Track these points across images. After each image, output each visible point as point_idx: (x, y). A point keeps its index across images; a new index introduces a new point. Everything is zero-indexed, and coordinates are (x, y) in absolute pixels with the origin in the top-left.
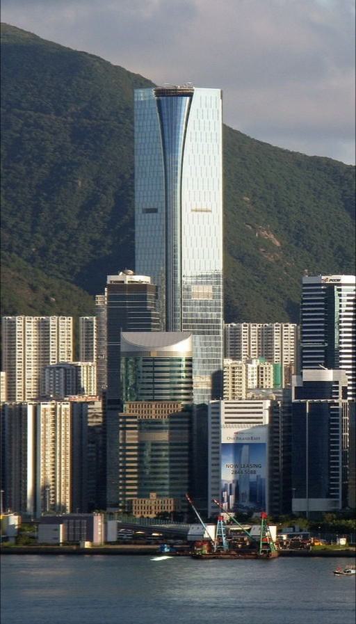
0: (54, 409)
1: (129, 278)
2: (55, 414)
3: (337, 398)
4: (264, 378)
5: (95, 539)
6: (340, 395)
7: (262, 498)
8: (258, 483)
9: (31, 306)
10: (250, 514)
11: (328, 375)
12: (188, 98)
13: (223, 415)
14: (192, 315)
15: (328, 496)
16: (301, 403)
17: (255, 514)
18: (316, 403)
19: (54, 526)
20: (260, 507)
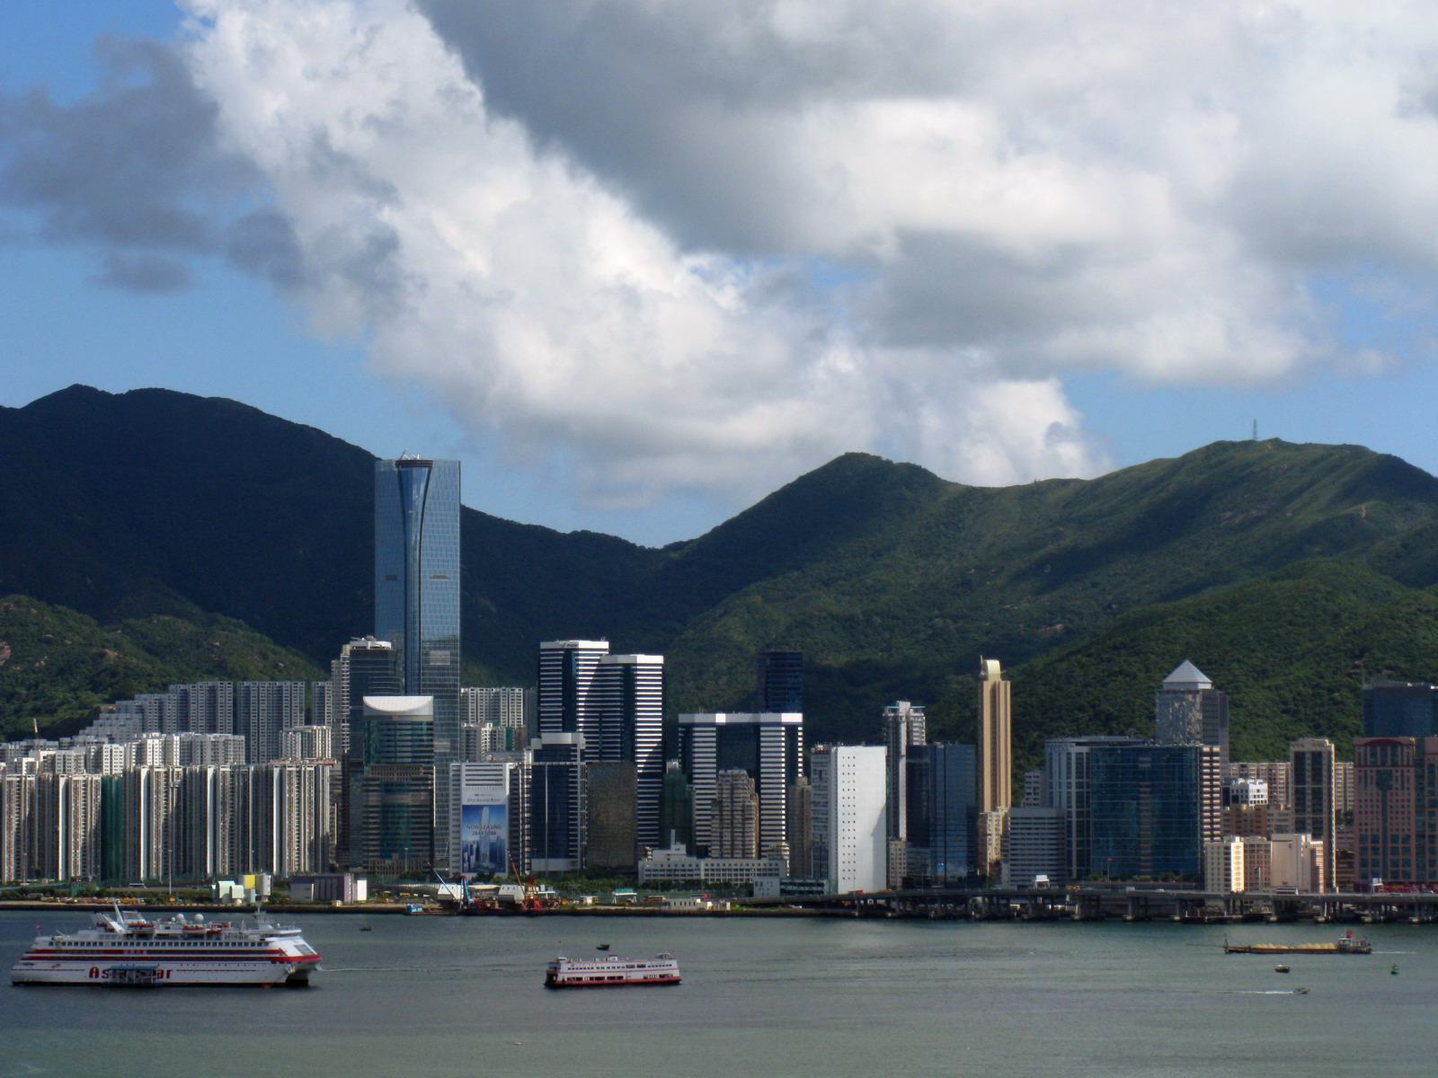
0: (299, 772)
1: (370, 643)
2: (299, 776)
3: (575, 761)
4: (497, 741)
5: (345, 897)
6: (579, 759)
7: (502, 858)
8: (498, 845)
9: (261, 672)
10: (492, 872)
11: (568, 738)
12: (427, 469)
13: (464, 778)
14: (430, 680)
15: (567, 856)
16: (540, 766)
17: (497, 875)
18: (555, 761)
19: (306, 886)
20: (501, 867)
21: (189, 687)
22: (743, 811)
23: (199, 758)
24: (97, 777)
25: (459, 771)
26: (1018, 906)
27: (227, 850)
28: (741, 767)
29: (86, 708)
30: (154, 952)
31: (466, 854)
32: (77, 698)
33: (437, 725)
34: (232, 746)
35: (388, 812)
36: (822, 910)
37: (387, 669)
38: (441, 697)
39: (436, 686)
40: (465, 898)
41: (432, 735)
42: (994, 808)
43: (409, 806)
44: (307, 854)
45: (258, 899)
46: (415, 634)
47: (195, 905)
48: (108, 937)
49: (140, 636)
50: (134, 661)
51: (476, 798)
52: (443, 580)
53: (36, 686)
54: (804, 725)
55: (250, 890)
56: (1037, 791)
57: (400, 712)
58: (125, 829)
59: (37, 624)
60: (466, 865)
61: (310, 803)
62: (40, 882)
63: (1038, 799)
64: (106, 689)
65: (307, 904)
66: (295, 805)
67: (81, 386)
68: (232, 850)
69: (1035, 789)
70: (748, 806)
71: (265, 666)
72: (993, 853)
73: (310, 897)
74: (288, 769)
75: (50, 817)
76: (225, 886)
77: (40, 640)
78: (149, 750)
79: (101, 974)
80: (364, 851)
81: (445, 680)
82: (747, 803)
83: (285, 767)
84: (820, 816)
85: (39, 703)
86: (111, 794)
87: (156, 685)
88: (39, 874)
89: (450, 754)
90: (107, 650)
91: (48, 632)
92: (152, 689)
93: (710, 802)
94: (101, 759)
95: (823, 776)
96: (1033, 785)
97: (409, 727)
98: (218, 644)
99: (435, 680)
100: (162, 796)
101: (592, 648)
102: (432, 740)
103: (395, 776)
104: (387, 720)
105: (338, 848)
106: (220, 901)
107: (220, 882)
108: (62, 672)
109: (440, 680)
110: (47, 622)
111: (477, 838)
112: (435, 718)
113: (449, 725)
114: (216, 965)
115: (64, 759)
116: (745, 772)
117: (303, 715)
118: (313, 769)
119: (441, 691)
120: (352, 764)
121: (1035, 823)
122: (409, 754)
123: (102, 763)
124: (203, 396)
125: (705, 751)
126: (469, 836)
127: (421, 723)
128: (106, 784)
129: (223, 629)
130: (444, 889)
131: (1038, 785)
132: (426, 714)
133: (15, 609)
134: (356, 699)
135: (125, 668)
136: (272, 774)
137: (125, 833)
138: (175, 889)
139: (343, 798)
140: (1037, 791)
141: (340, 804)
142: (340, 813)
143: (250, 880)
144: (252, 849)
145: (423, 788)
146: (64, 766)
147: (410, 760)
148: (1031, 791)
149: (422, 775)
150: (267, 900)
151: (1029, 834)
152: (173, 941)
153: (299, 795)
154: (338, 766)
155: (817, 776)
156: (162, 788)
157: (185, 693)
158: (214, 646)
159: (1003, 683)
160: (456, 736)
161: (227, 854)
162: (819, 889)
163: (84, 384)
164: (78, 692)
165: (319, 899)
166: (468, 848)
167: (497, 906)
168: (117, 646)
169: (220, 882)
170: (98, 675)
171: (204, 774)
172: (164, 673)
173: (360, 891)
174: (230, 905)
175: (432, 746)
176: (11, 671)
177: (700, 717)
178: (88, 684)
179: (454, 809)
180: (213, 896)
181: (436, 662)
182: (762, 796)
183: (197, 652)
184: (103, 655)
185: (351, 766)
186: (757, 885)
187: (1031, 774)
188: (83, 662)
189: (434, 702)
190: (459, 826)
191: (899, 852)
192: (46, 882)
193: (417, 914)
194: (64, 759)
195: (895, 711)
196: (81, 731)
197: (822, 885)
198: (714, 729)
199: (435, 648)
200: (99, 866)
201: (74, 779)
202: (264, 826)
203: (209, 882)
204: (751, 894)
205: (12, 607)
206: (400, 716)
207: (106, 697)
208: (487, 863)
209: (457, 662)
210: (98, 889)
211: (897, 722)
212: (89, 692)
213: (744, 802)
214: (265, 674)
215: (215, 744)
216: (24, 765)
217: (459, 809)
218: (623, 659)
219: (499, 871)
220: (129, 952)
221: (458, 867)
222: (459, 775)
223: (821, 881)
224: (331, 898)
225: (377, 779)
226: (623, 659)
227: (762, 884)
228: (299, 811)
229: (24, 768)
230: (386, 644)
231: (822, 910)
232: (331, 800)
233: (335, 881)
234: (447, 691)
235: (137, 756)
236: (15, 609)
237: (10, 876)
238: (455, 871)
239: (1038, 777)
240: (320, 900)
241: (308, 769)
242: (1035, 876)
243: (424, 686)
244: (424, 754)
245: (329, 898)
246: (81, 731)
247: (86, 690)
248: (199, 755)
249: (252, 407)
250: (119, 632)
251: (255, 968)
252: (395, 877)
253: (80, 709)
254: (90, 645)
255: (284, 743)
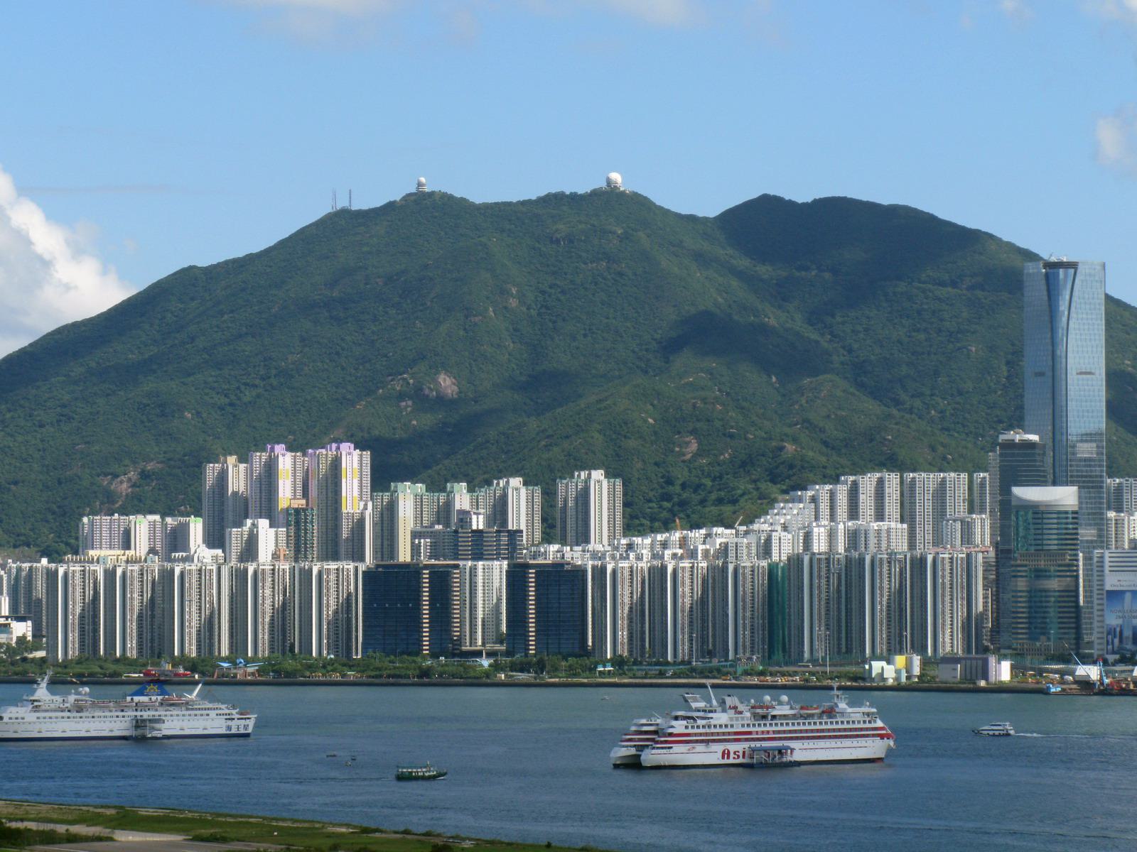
1: (1018, 436)
2: (952, 562)
14: (1077, 471)
19: (953, 666)
21: (860, 478)
23: (863, 546)
24: (764, 563)
25: (1102, 557)
27: (884, 632)
29: (765, 498)
30: (779, 732)
31: (1110, 637)
32: (758, 489)
33: (1084, 514)
35: (1036, 598)
37: (1035, 461)
38: (1084, 487)
39: (1082, 476)
40: (1101, 681)
41: (1077, 523)
43: (1055, 591)
44: (960, 636)
45: (908, 678)
46: (1062, 427)
47: (849, 684)
48: (737, 719)
49: (818, 430)
50: (811, 454)
51: (1118, 583)
52: (1088, 376)
53: (721, 477)
55: (900, 670)
57: (1046, 501)
58: (789, 612)
59: (722, 420)
60: (1110, 647)
61: (962, 588)
62: (710, 662)
64: (783, 480)
65: (954, 683)
66: (948, 590)
67: (769, 195)
68: (889, 632)
71: (934, 458)
73: (956, 677)
74: (941, 556)
75: (721, 599)
76: (877, 666)
77: (724, 435)
78: (815, 538)
79: (732, 755)
80: (1013, 633)
81: (1091, 471)
83: (938, 553)
85: (723, 493)
86: (777, 579)
87: (831, 477)
88: (711, 654)
89: (1096, 541)
90: (786, 444)
91: (732, 428)
92: (826, 480)
94: (771, 546)
97: (1055, 516)
98: (890, 437)
99: (1082, 471)
100: (824, 581)
102: (1076, 529)
103: (1043, 562)
104: (1038, 512)
105: (992, 631)
106: (873, 680)
107: (872, 662)
108: (743, 464)
109: (1087, 471)
110: (731, 417)
111: (1120, 622)
112: (1080, 508)
113: (1094, 514)
114: (832, 743)
115: (737, 546)
117: (966, 504)
118: (964, 556)
119: (1084, 482)
122: (1056, 542)
123: (771, 550)
124: (884, 203)
126: (1113, 620)
127: (1066, 512)
128: (772, 569)
129: (896, 424)
130: (1082, 670)
132: (1071, 503)
133: (702, 406)
134: (1005, 489)
135: (802, 460)
136: (802, 561)
137: (790, 616)
138: (834, 669)
139: (997, 584)
141: (994, 589)
142: (994, 598)
143: (900, 660)
144: (906, 629)
145: (1068, 574)
146: (736, 553)
147: (1056, 547)
149: (1067, 561)
150: (916, 680)
152: (785, 722)
153: (952, 581)
154: (992, 554)
156: (823, 573)
157: (855, 484)
158: (885, 439)
160: (1103, 525)
161: (884, 636)
163: (772, 194)
164: (758, 483)
165: (965, 679)
166: (1111, 631)
167: (1132, 687)
168: (795, 440)
169: (872, 662)
170: (777, 467)
171: (310, 570)
172: (838, 466)
173: (1003, 671)
174: (881, 684)
175: (1077, 534)
176: (697, 464)
178: (768, 475)
179: (1098, 594)
180: (867, 676)
181: (1083, 453)
183: (870, 445)
184: (782, 449)
185: (1003, 553)
188: (763, 455)
189: (1079, 492)
190: (1103, 610)
192: (715, 662)
193: (1056, 694)
194: (737, 546)
196: (756, 520)
199: (1082, 441)
200: (766, 647)
201: (742, 565)
203: (864, 661)
205: (699, 404)
206: (1046, 506)
207: (784, 487)
209: (1103, 454)
210: (761, 668)
212: (768, 483)
214: (934, 466)
215: (879, 532)
216: (700, 552)
217: (1102, 594)
220: (757, 733)
221: (1102, 650)
222: (1102, 562)
224: (977, 679)
225: (1026, 566)
228: (952, 595)
229: (700, 555)
230: (1034, 438)
232: (984, 586)
233: (980, 662)
234: (1093, 482)
235: (804, 543)
236: (702, 406)
237: (684, 655)
238: (1100, 653)
240: (966, 679)
241: (960, 556)
243: (1072, 476)
244: (1070, 541)
245: (974, 677)
246: (756, 520)
247: (766, 481)
248: (863, 542)
249: (928, 213)
250: (799, 426)
251: (866, 745)
252: (1042, 658)
253: (760, 499)
254: (771, 439)
255: (944, 532)
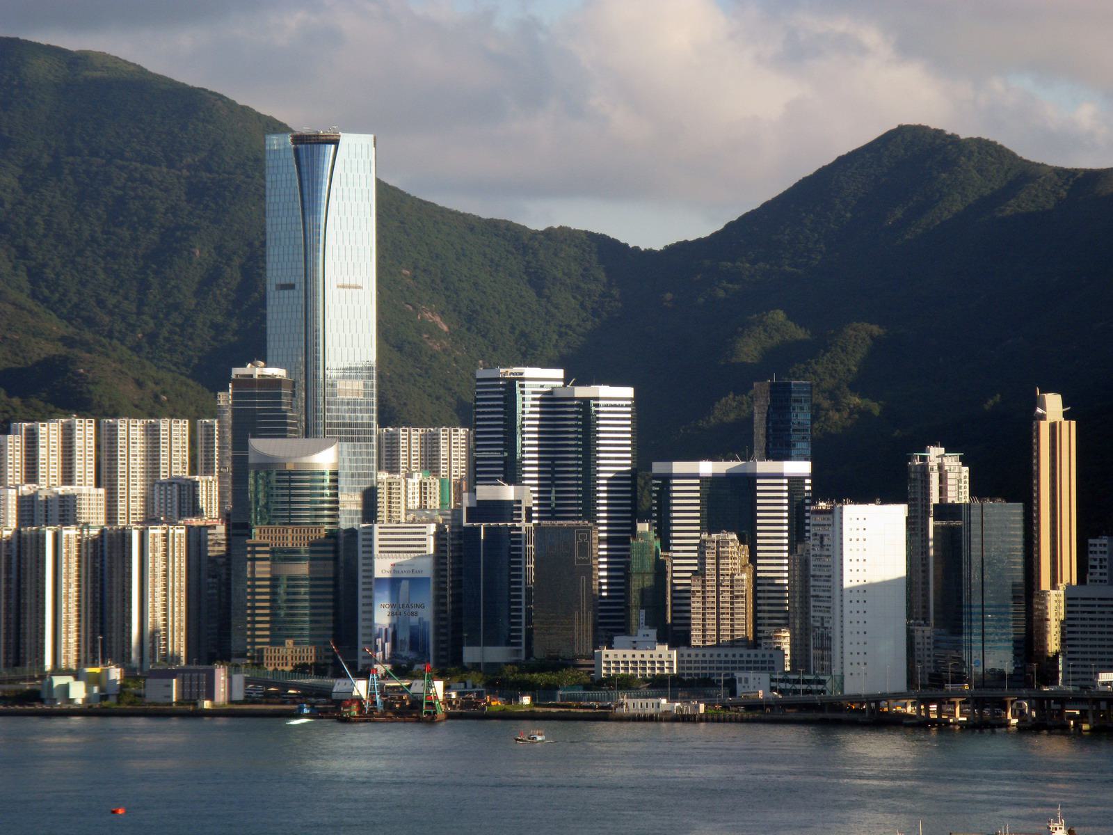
1: (259, 370)
2: (166, 540)
3: (519, 521)
4: (428, 496)
7: (426, 646)
8: (421, 628)
9: (136, 406)
10: (411, 666)
11: (508, 492)
12: (333, 146)
13: (376, 543)
15: (508, 644)
17: (417, 667)
19: (165, 681)
22: (732, 587)
26: (1078, 712)
28: (730, 530)
34: (87, 502)
36: (820, 715)
42: (1054, 586)
54: (813, 476)
56: (1104, 563)
63: (1105, 574)
69: (1101, 560)
70: (738, 580)
72: (1053, 644)
82: (736, 577)
84: (821, 594)
93: (689, 575)
95: (826, 541)
96: (1099, 556)
101: (539, 380)
116: (734, 536)
120: (236, 526)
121: (1099, 606)
125: (686, 508)
131: (1106, 556)
140: (1104, 563)
148: (1096, 563)
151: (1091, 619)
155: (818, 542)
159: (1065, 424)
162: (820, 687)
177: (678, 467)
182: (759, 568)
186: (740, 682)
187: (1097, 541)
191: (926, 640)
195: (924, 459)
197: (823, 682)
198: (698, 481)
200: (11, 641)
202: (119, 605)
204: (733, 693)
208: (405, 652)
211: (924, 472)
213: (733, 575)
218: (581, 392)
219: (421, 662)
223: (822, 678)
225: (267, 545)
226: (581, 392)
227: (747, 680)
231: (820, 715)
239: (1105, 545)
242: (1096, 674)
